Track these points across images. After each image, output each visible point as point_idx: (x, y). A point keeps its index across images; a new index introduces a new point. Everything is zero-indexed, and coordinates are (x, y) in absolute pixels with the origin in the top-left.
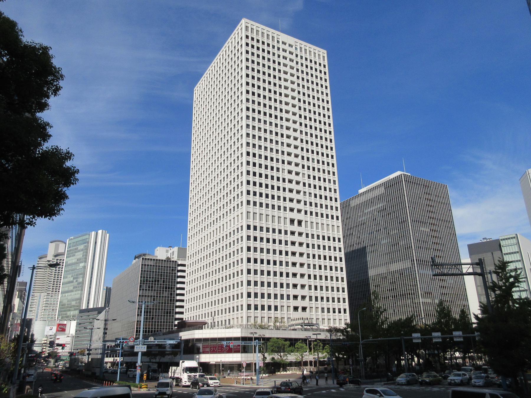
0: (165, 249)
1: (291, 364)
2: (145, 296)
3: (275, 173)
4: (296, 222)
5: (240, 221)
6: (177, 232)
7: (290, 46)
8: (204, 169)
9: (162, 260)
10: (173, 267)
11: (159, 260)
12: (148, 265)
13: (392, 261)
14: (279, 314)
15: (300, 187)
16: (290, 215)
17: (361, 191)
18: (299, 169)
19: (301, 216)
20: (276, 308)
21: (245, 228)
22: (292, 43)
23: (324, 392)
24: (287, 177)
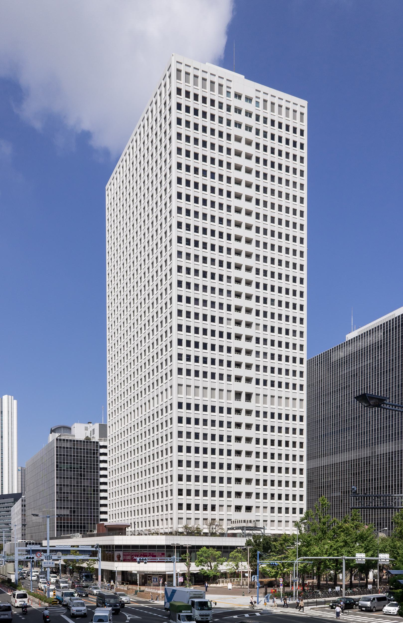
0: (83, 426)
1: (224, 575)
2: (67, 478)
3: (217, 326)
4: (243, 396)
5: (169, 397)
6: (95, 409)
7: (249, 99)
8: (127, 314)
9: (81, 441)
10: (94, 450)
11: (77, 441)
12: (64, 448)
13: (379, 441)
14: (217, 515)
15: (252, 346)
16: (236, 386)
17: (350, 336)
18: (251, 317)
19: (251, 388)
20: (213, 508)
21: (175, 406)
22: (252, 94)
23: (235, 617)
24: (235, 330)
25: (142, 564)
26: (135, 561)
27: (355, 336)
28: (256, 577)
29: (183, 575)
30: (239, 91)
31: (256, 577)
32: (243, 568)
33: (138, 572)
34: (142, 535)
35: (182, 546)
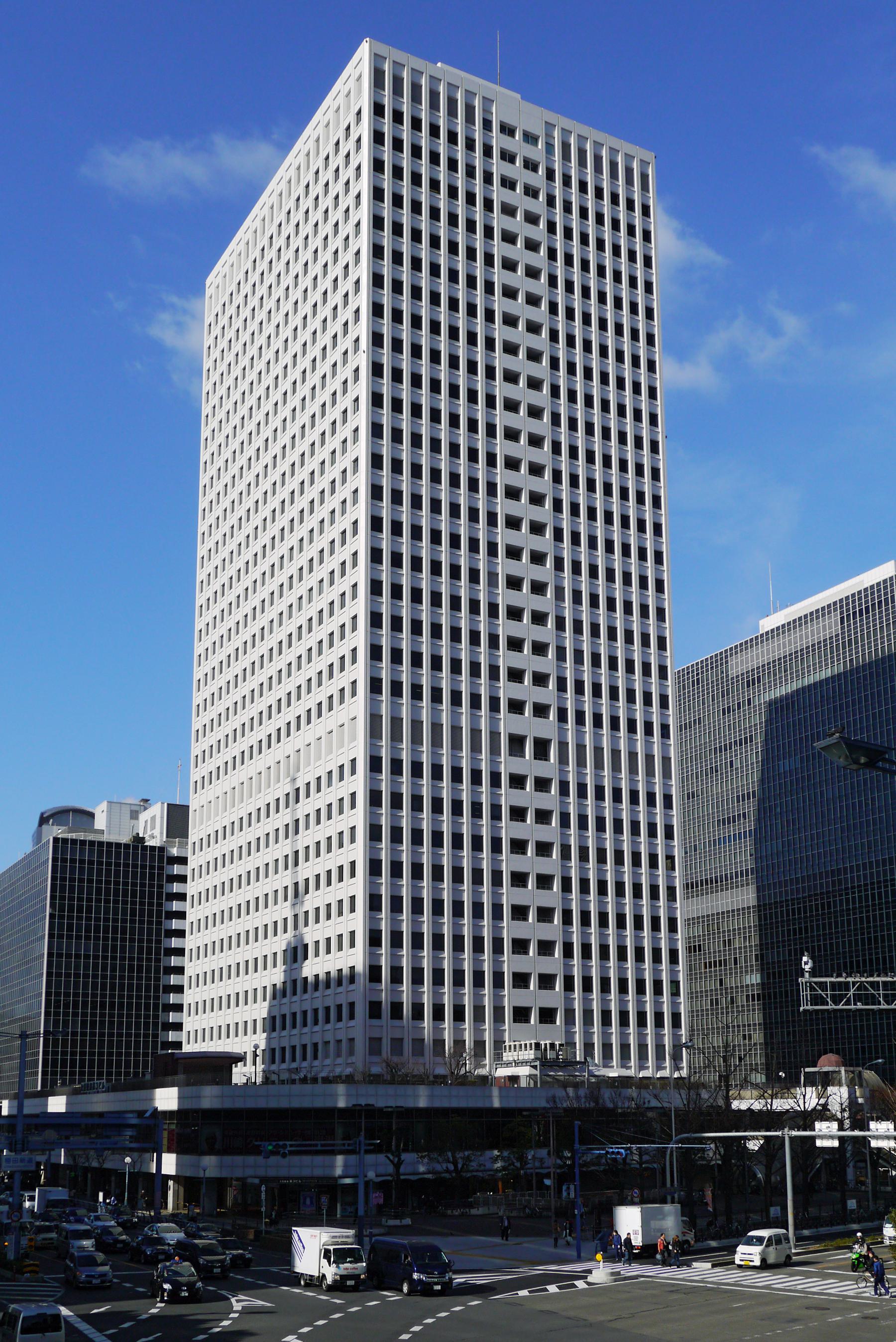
7: (530, 138)
9: (118, 845)
11: (109, 844)
17: (768, 624)
22: (538, 130)
23: (524, 1293)
25: (273, 1159)
26: (256, 1151)
27: (780, 624)
28: (572, 1187)
29: (383, 1186)
30: (510, 121)
31: (572, 1187)
32: (537, 1164)
33: (264, 1180)
34: (273, 1083)
35: (380, 1110)
